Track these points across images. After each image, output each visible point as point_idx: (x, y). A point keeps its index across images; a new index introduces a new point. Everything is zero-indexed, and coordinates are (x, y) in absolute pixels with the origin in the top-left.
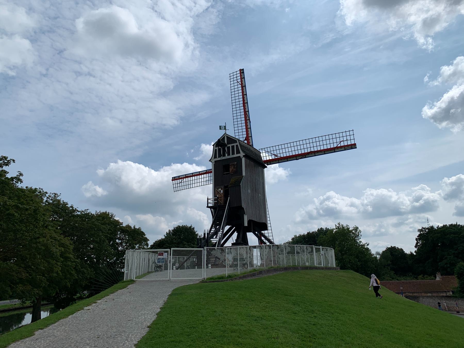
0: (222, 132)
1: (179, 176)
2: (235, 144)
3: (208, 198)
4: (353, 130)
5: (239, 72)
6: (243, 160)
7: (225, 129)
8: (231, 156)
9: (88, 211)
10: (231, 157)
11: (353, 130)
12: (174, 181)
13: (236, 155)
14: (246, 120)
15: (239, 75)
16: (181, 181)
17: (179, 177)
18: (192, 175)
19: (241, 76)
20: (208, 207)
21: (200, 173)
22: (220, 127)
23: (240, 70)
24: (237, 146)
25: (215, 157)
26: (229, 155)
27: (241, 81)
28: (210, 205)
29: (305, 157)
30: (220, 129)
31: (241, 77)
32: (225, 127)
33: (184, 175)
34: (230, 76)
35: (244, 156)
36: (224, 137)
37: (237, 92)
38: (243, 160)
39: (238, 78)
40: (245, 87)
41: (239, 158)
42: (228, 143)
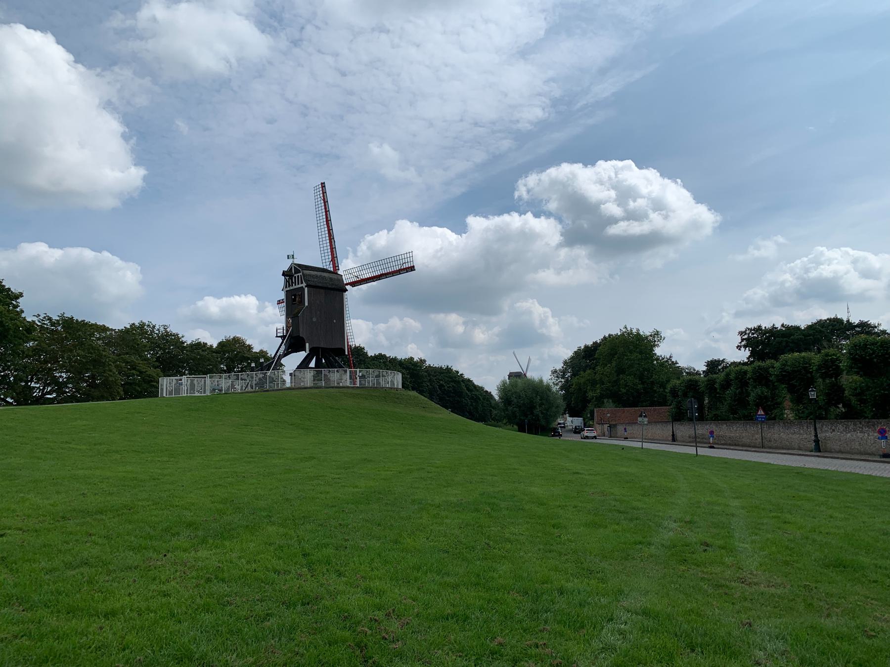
0: (290, 261)
2: (299, 274)
5: (320, 186)
6: (306, 289)
7: (293, 258)
8: (297, 286)
9: (200, 340)
12: (412, 265)
13: (300, 286)
14: (330, 240)
15: (321, 189)
19: (323, 190)
20: (277, 337)
22: (288, 256)
24: (301, 275)
25: (286, 287)
26: (295, 285)
28: (279, 335)
29: (366, 282)
30: (288, 258)
31: (323, 191)
32: (293, 256)
35: (306, 286)
38: (306, 289)
41: (302, 289)
42: (295, 273)
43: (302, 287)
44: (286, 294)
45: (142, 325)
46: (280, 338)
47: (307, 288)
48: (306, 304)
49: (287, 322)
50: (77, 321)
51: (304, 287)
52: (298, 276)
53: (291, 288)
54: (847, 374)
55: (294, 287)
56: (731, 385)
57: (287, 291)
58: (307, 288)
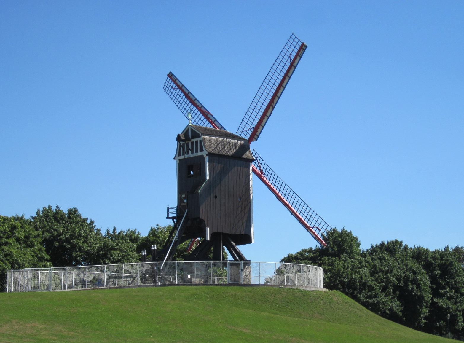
1: (301, 57)
3: (168, 208)
4: (293, 34)
5: (169, 79)
8: (195, 155)
10: (195, 156)
11: (293, 34)
13: (199, 154)
16: (291, 58)
17: (299, 56)
18: (257, 135)
20: (168, 218)
21: (287, 78)
23: (168, 75)
25: (179, 155)
27: (177, 84)
28: (170, 215)
33: (297, 65)
34: (328, 225)
36: (188, 129)
37: (308, 217)
39: (174, 87)
40: (216, 121)
42: (193, 137)
43: (202, 156)
44: (179, 164)
45: (356, 239)
46: (171, 220)
47: (208, 157)
48: (208, 178)
49: (180, 200)
50: (406, 248)
51: (205, 156)
52: (197, 142)
53: (187, 156)
54: (360, 294)
55: (190, 155)
56: (51, 233)
57: (180, 160)
58: (208, 157)
